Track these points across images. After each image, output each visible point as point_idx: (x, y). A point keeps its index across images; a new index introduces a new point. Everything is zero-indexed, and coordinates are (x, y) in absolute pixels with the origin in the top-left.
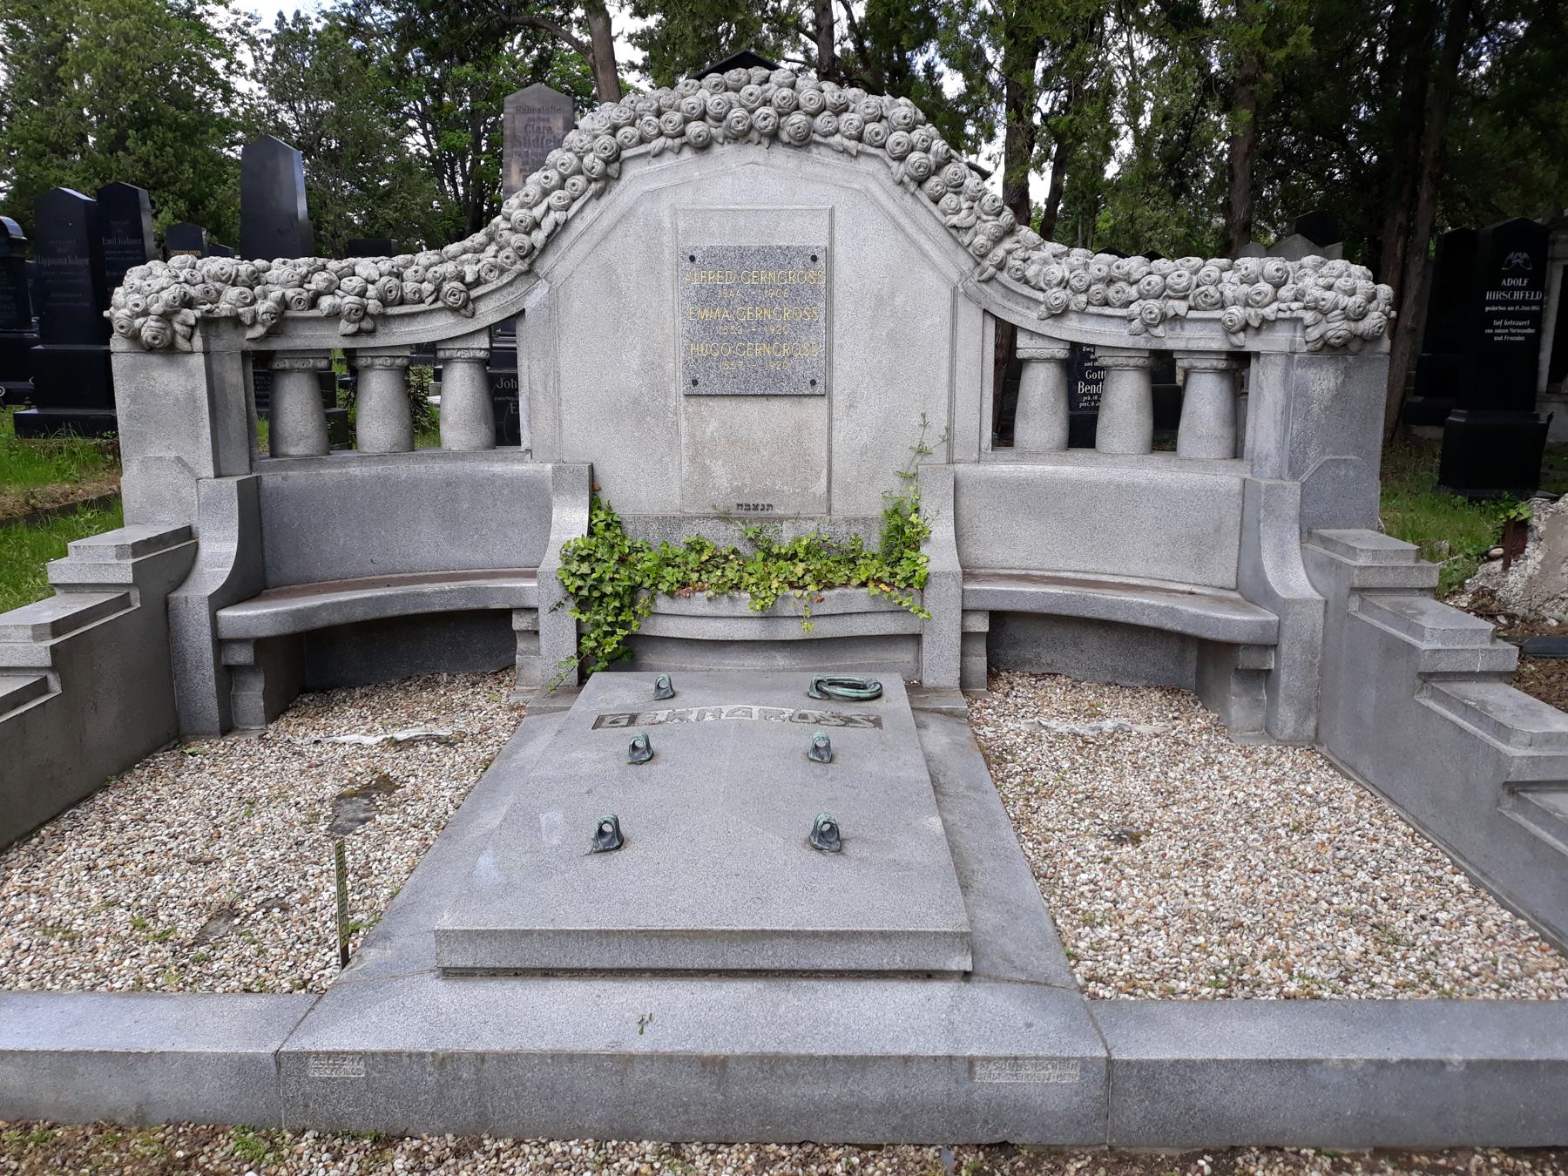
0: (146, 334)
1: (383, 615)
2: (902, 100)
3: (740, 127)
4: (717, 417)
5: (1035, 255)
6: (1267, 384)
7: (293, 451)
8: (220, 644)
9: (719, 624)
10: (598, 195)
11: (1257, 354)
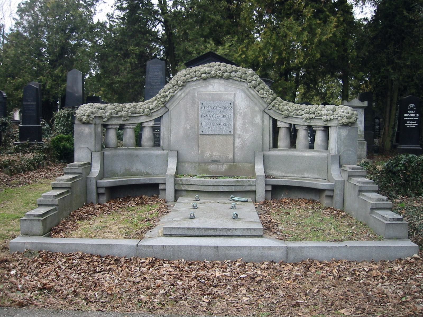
0: (84, 120)
2: (250, 69)
3: (214, 75)
6: (333, 134)
8: (98, 188)
9: (203, 187)
10: (181, 90)
11: (330, 126)
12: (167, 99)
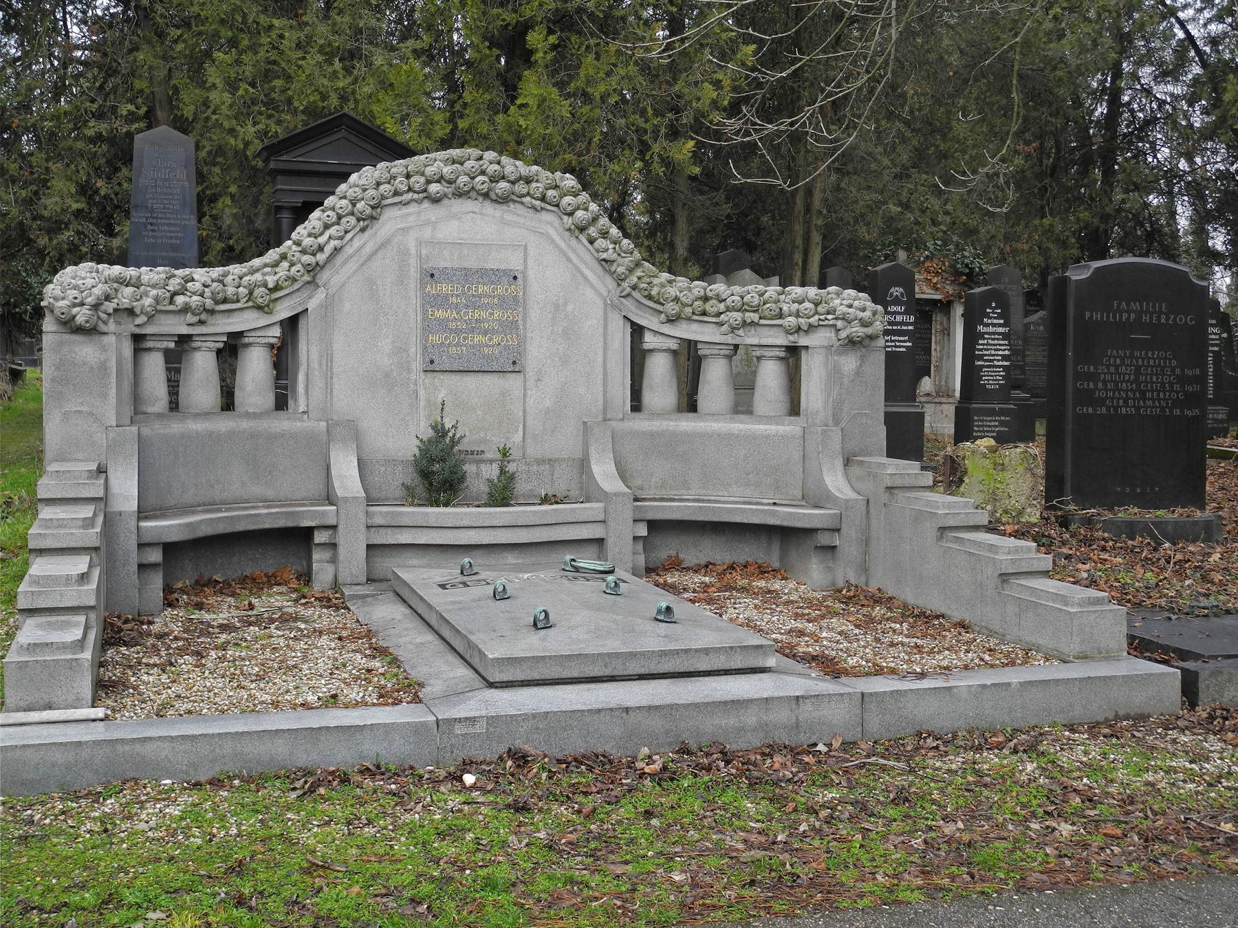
1: (235, 530)
4: (444, 388)
5: (656, 281)
6: (814, 370)
7: (150, 410)
8: (141, 546)
9: (472, 533)
10: (363, 230)
11: (807, 347)
12: (321, 257)
